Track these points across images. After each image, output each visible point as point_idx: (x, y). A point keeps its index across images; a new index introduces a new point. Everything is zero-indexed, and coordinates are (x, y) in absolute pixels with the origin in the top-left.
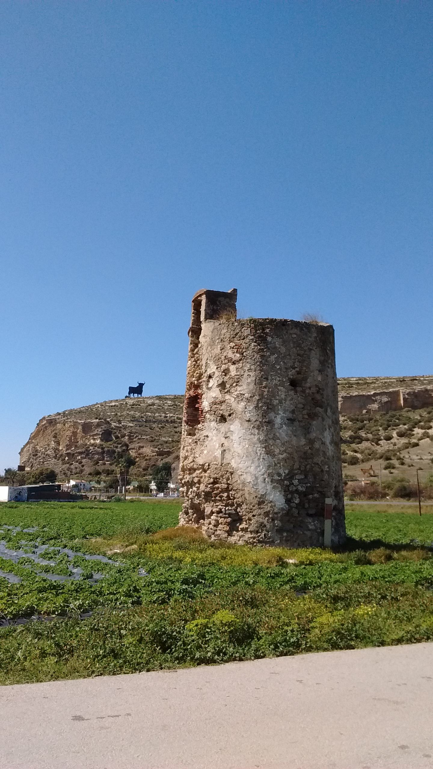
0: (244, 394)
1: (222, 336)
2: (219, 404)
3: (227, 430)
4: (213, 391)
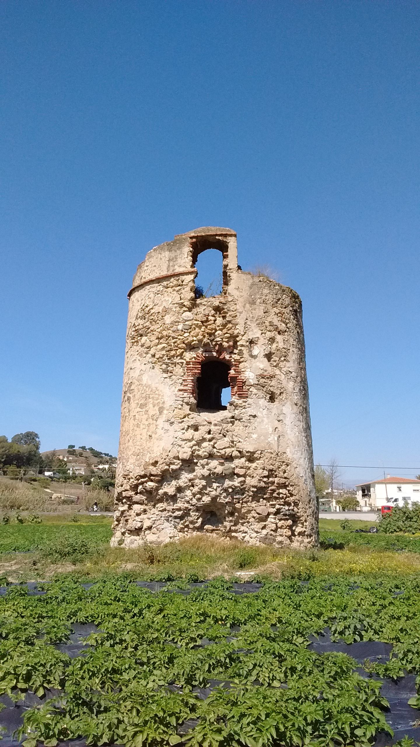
0: (291, 372)
1: (264, 297)
2: (268, 378)
3: (279, 412)
4: (260, 361)
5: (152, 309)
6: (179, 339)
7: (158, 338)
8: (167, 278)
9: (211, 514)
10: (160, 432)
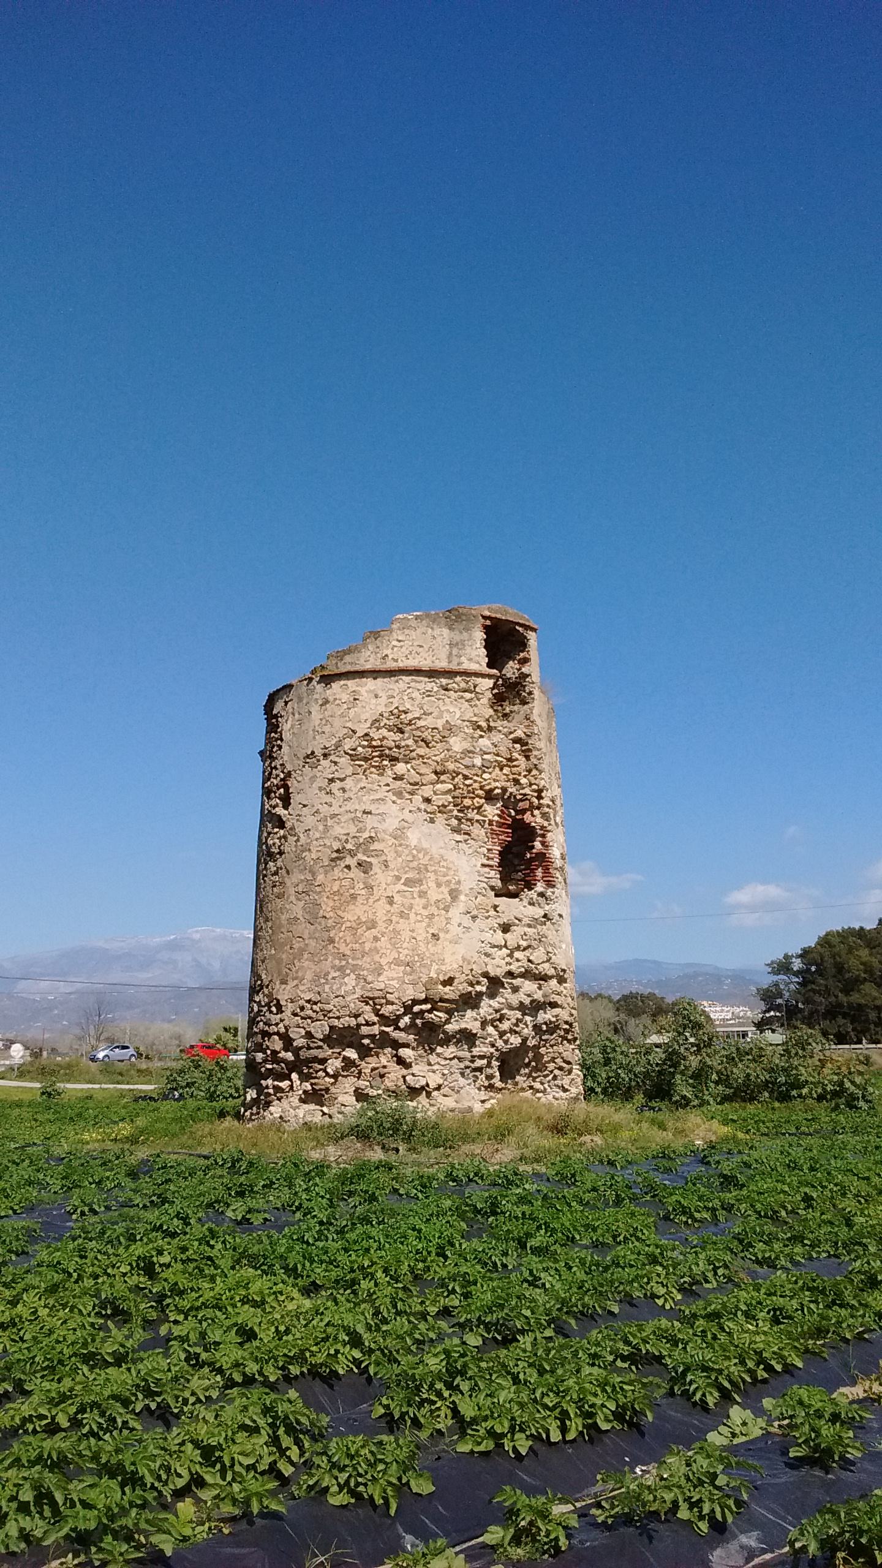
5: (419, 719)
6: (475, 781)
7: (436, 773)
8: (450, 674)
9: (510, 1064)
10: (454, 929)
